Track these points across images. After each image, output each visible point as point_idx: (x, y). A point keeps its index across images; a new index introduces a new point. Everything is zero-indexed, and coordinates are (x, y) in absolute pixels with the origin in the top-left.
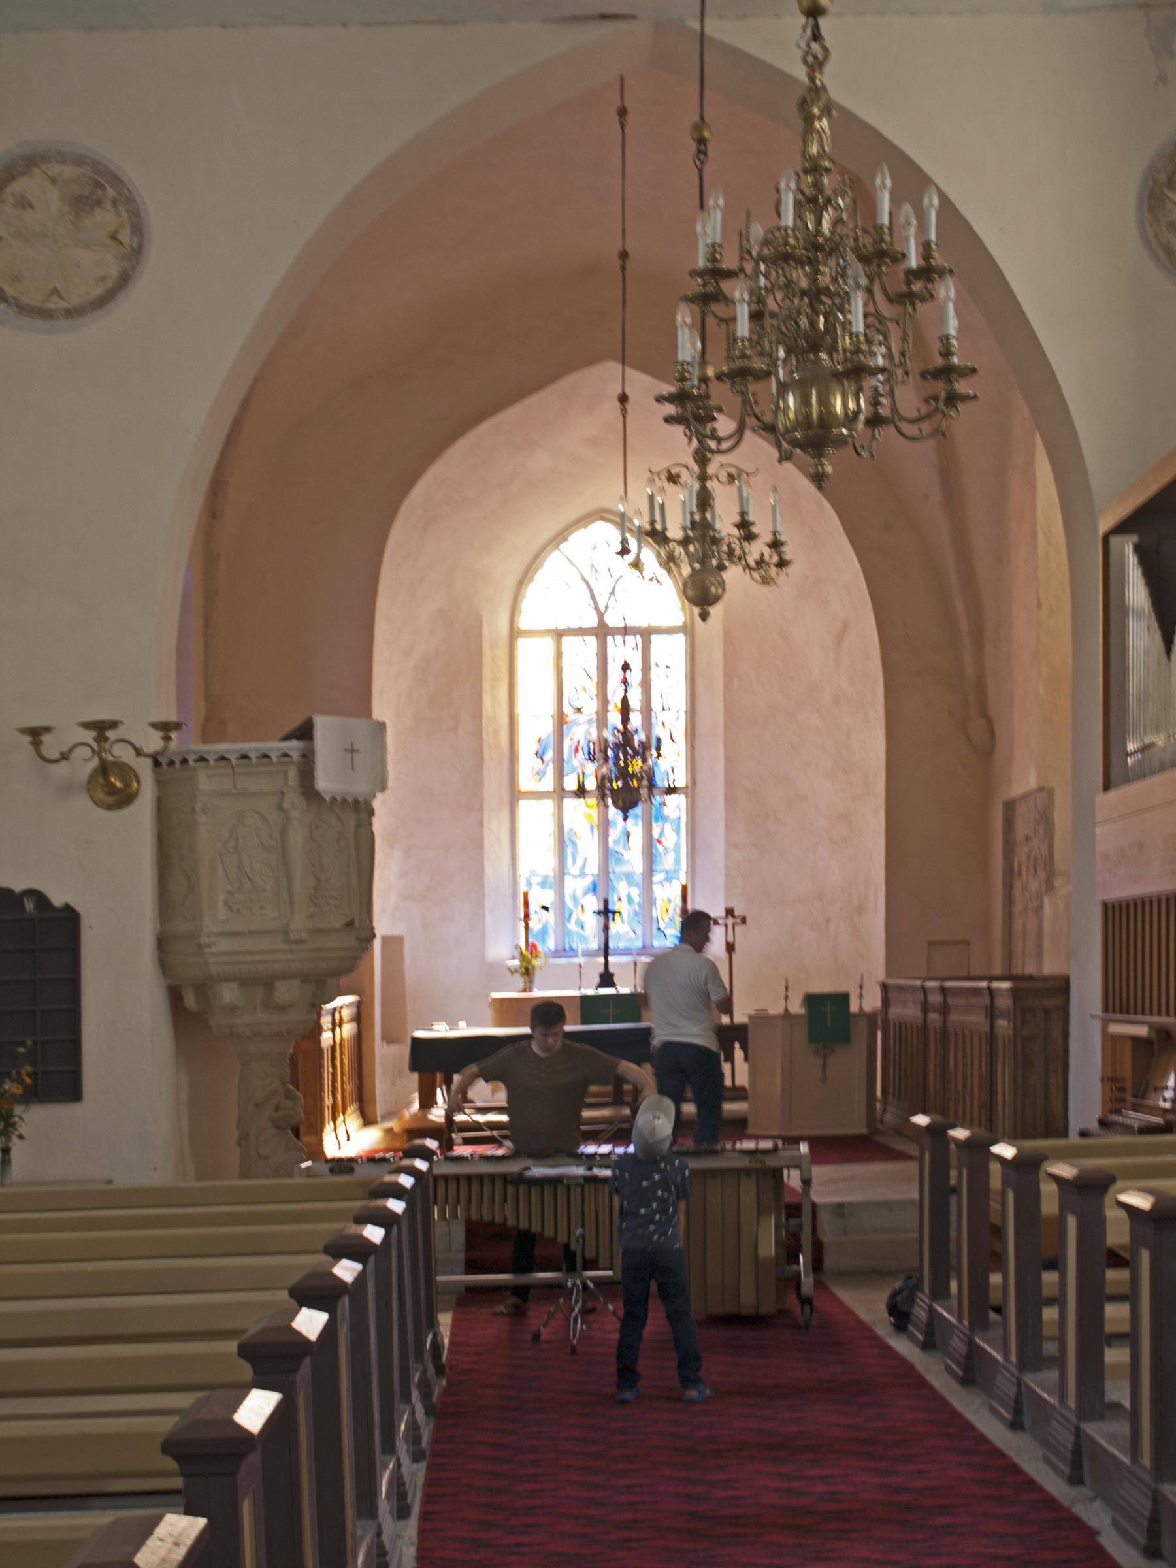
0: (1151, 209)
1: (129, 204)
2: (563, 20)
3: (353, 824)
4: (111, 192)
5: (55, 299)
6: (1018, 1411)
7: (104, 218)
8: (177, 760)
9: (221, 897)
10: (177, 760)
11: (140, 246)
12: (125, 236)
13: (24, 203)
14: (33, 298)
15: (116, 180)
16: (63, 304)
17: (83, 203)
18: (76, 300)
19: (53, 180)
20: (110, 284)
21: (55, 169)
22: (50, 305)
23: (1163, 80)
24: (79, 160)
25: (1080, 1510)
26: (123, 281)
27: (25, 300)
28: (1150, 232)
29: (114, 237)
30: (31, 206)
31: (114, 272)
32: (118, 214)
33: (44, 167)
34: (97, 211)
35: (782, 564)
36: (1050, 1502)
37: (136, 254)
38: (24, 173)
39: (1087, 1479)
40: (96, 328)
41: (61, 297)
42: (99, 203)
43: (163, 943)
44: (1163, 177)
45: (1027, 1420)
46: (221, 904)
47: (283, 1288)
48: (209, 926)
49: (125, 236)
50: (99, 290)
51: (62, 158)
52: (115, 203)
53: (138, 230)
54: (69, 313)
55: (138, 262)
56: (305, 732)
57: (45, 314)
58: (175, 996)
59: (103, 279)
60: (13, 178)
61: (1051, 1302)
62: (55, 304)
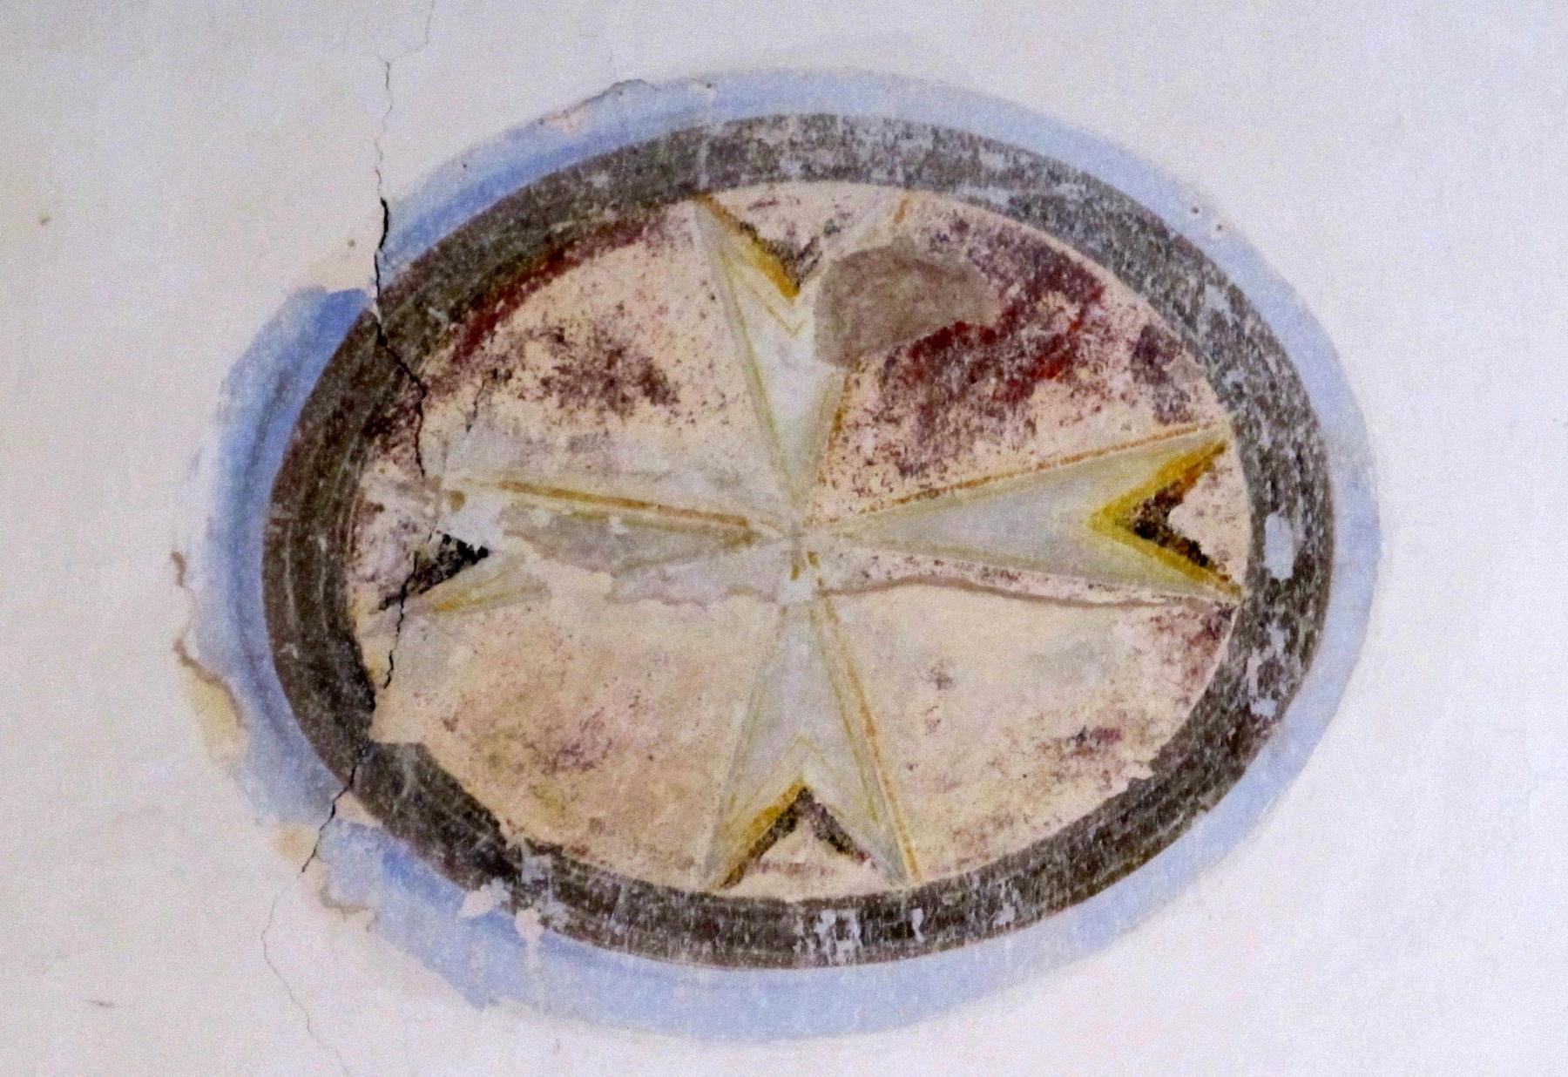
4: (1125, 306)
7: (1093, 435)
11: (1312, 567)
13: (615, 378)
15: (1154, 248)
16: (851, 879)
18: (931, 858)
19: (789, 262)
20: (1133, 764)
21: (799, 208)
22: (755, 886)
24: (943, 162)
26: (1217, 750)
27: (621, 861)
29: (1150, 525)
30: (654, 386)
31: (1159, 699)
32: (1173, 413)
33: (736, 200)
34: (1047, 397)
37: (1295, 601)
38: (622, 233)
41: (838, 842)
42: (1057, 360)
49: (1216, 515)
50: (1079, 800)
51: (836, 152)
52: (1148, 353)
53: (1292, 481)
54: (886, 925)
55: (1303, 648)
59: (1094, 741)
60: (557, 260)
62: (797, 874)
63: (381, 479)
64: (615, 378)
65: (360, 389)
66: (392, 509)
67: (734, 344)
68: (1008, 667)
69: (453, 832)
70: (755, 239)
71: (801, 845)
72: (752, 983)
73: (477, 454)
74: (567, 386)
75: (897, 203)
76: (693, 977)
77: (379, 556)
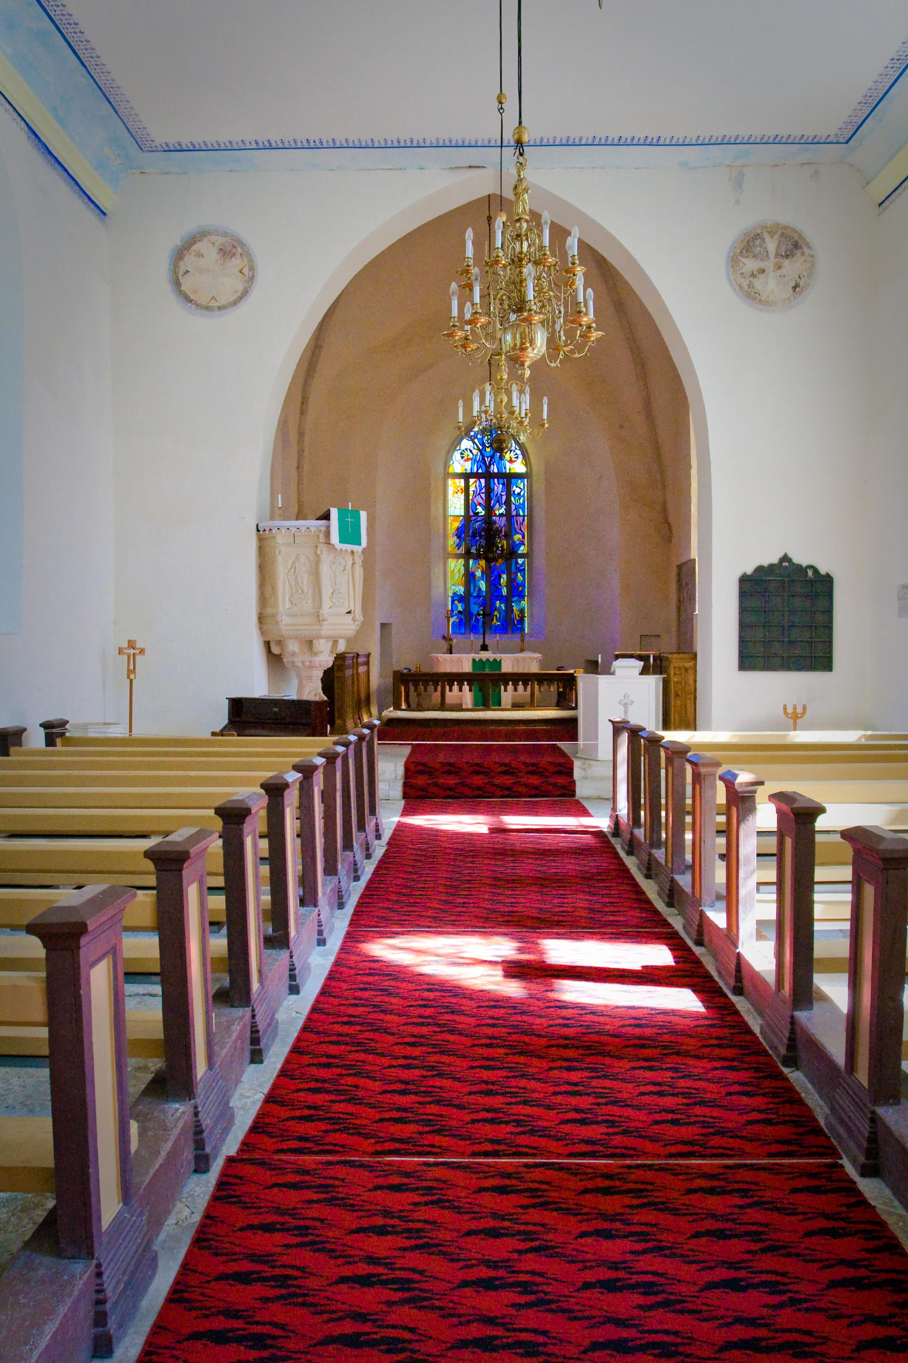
0: (732, 266)
1: (247, 255)
2: (452, 168)
3: (351, 562)
4: (239, 250)
5: (213, 301)
6: (649, 869)
7: (237, 263)
8: (267, 529)
9: (287, 598)
10: (267, 529)
11: (253, 276)
12: (246, 271)
14: (203, 301)
15: (242, 244)
16: (217, 304)
17: (226, 253)
18: (222, 302)
19: (213, 244)
20: (239, 294)
21: (214, 238)
23: (738, 202)
24: (225, 234)
25: (670, 920)
26: (245, 293)
27: (199, 302)
28: (732, 277)
31: (240, 288)
32: (243, 261)
33: (209, 237)
35: (142, 651)
36: (656, 912)
37: (252, 279)
39: (676, 904)
40: (232, 317)
43: (261, 619)
44: (738, 251)
45: (653, 873)
46: (287, 600)
47: (209, 808)
48: (281, 609)
49: (246, 271)
50: (234, 297)
53: (252, 268)
54: (220, 308)
56: (326, 517)
57: (207, 308)
58: (267, 644)
61: (688, 813)
62: (213, 304)
63: (181, 264)
64: (200, 255)
65: (180, 254)
66: (182, 267)
67: (208, 249)
68: (228, 284)
69: (188, 299)
70: (197, 305)
71: (213, 301)
72: (209, 313)
73: (189, 261)
74: (195, 255)
75: (220, 920)
76: (205, 312)
77: (181, 273)
